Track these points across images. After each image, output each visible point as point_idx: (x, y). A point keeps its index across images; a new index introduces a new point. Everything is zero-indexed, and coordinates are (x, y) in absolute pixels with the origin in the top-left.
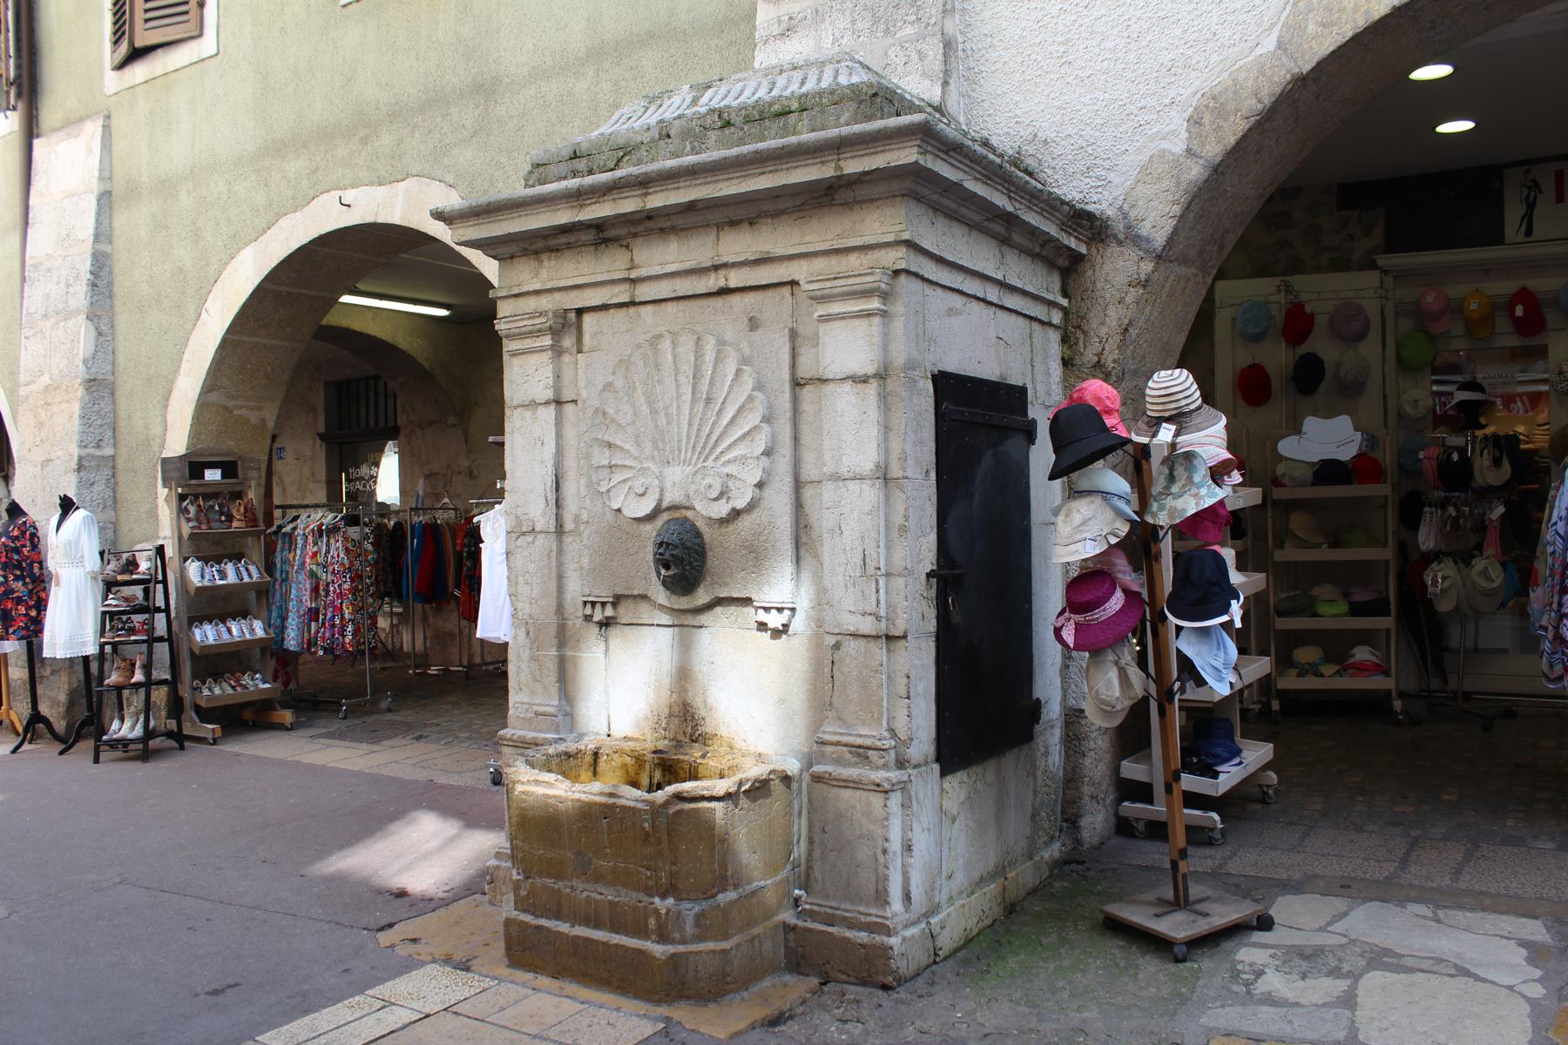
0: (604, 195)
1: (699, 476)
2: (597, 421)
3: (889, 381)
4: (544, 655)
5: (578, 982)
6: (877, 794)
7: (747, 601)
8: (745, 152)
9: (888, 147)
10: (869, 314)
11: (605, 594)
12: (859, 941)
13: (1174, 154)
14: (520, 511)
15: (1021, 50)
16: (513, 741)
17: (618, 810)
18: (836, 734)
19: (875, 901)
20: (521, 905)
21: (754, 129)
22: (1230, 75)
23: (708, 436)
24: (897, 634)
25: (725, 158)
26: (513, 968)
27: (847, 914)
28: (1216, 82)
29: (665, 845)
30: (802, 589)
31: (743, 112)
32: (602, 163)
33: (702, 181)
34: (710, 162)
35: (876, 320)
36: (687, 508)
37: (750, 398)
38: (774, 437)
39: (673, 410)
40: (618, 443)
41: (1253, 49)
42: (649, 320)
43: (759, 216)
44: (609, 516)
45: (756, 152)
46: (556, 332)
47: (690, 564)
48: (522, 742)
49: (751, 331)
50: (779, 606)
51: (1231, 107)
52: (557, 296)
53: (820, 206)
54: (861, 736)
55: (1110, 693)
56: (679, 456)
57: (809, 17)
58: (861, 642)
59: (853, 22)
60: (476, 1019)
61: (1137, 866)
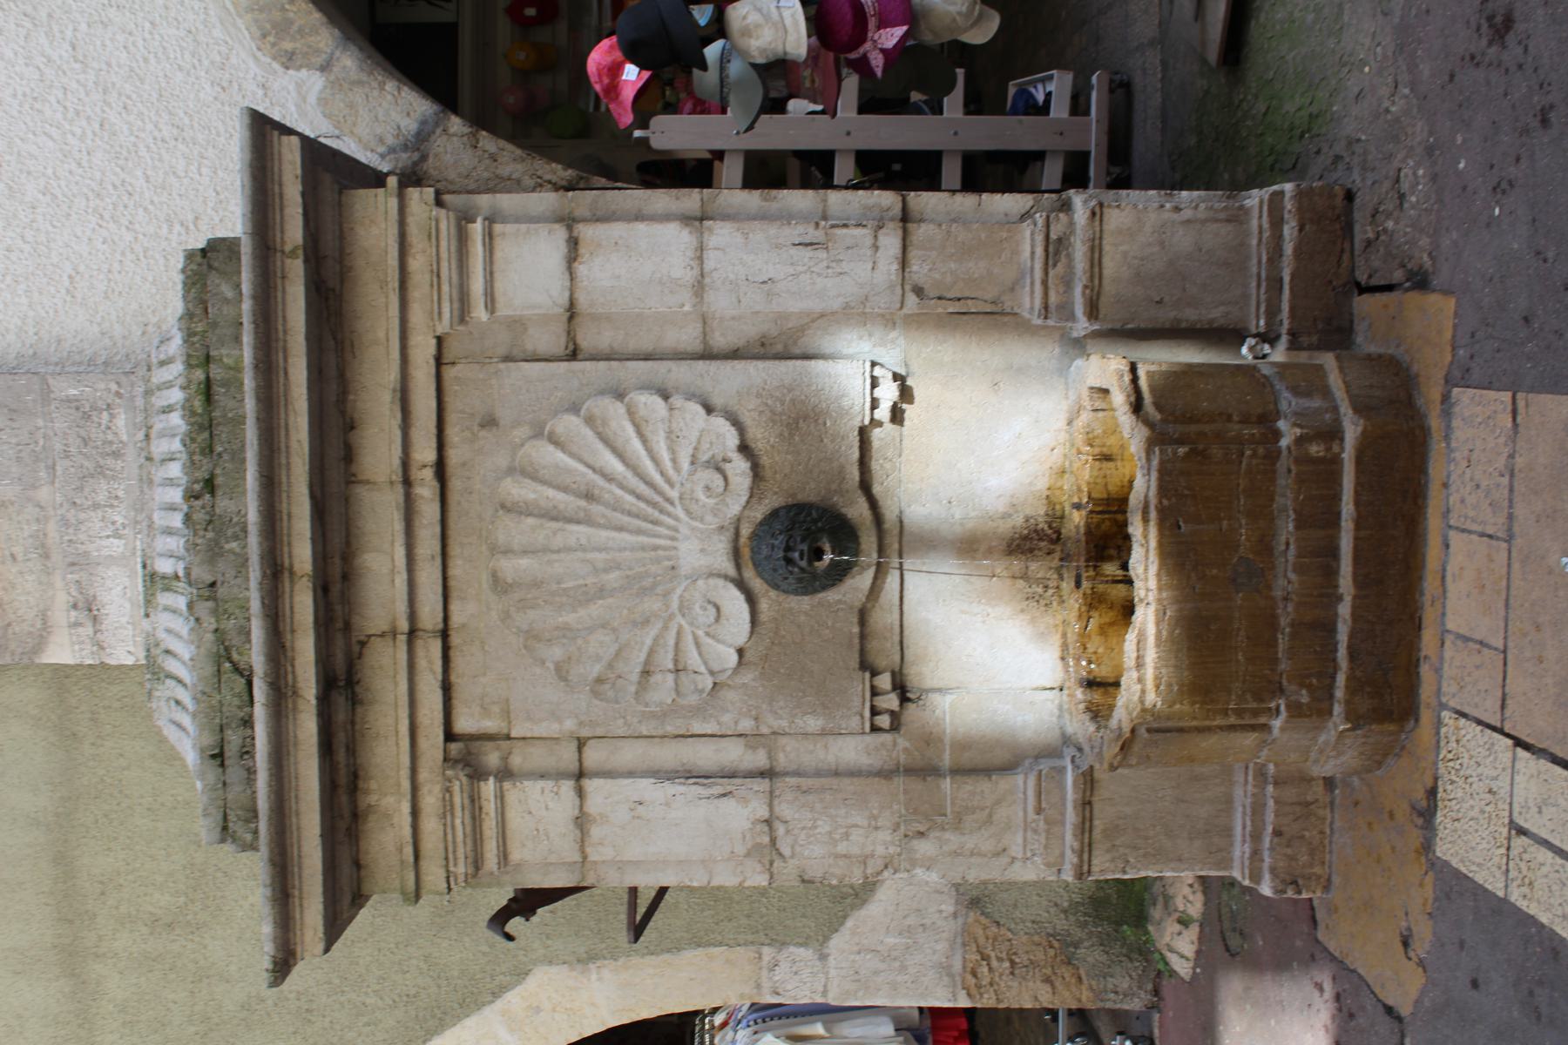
1: (694, 507)
2: (610, 694)
3: (577, 213)
4: (953, 804)
5: (1420, 578)
7: (863, 433)
9: (276, 178)
10: (489, 236)
11: (858, 686)
12: (1296, 233)
13: (325, 87)
14: (740, 849)
15: (170, 284)
17: (1165, 502)
18: (1032, 292)
20: (1320, 710)
21: (223, 432)
22: (240, 16)
25: (258, 419)
28: (246, 33)
29: (1207, 428)
30: (849, 17)
31: (197, 458)
32: (236, 702)
33: (284, 472)
34: (260, 444)
35: (498, 228)
36: (737, 534)
37: (590, 421)
38: (646, 387)
40: (643, 656)
43: (343, 413)
44: (747, 677)
45: (256, 367)
46: (477, 774)
47: (815, 521)
50: (868, 381)
51: (277, 15)
52: (424, 775)
54: (1033, 253)
56: (665, 548)
57: (76, 577)
58: (913, 253)
59: (96, 506)
60: (1505, 664)
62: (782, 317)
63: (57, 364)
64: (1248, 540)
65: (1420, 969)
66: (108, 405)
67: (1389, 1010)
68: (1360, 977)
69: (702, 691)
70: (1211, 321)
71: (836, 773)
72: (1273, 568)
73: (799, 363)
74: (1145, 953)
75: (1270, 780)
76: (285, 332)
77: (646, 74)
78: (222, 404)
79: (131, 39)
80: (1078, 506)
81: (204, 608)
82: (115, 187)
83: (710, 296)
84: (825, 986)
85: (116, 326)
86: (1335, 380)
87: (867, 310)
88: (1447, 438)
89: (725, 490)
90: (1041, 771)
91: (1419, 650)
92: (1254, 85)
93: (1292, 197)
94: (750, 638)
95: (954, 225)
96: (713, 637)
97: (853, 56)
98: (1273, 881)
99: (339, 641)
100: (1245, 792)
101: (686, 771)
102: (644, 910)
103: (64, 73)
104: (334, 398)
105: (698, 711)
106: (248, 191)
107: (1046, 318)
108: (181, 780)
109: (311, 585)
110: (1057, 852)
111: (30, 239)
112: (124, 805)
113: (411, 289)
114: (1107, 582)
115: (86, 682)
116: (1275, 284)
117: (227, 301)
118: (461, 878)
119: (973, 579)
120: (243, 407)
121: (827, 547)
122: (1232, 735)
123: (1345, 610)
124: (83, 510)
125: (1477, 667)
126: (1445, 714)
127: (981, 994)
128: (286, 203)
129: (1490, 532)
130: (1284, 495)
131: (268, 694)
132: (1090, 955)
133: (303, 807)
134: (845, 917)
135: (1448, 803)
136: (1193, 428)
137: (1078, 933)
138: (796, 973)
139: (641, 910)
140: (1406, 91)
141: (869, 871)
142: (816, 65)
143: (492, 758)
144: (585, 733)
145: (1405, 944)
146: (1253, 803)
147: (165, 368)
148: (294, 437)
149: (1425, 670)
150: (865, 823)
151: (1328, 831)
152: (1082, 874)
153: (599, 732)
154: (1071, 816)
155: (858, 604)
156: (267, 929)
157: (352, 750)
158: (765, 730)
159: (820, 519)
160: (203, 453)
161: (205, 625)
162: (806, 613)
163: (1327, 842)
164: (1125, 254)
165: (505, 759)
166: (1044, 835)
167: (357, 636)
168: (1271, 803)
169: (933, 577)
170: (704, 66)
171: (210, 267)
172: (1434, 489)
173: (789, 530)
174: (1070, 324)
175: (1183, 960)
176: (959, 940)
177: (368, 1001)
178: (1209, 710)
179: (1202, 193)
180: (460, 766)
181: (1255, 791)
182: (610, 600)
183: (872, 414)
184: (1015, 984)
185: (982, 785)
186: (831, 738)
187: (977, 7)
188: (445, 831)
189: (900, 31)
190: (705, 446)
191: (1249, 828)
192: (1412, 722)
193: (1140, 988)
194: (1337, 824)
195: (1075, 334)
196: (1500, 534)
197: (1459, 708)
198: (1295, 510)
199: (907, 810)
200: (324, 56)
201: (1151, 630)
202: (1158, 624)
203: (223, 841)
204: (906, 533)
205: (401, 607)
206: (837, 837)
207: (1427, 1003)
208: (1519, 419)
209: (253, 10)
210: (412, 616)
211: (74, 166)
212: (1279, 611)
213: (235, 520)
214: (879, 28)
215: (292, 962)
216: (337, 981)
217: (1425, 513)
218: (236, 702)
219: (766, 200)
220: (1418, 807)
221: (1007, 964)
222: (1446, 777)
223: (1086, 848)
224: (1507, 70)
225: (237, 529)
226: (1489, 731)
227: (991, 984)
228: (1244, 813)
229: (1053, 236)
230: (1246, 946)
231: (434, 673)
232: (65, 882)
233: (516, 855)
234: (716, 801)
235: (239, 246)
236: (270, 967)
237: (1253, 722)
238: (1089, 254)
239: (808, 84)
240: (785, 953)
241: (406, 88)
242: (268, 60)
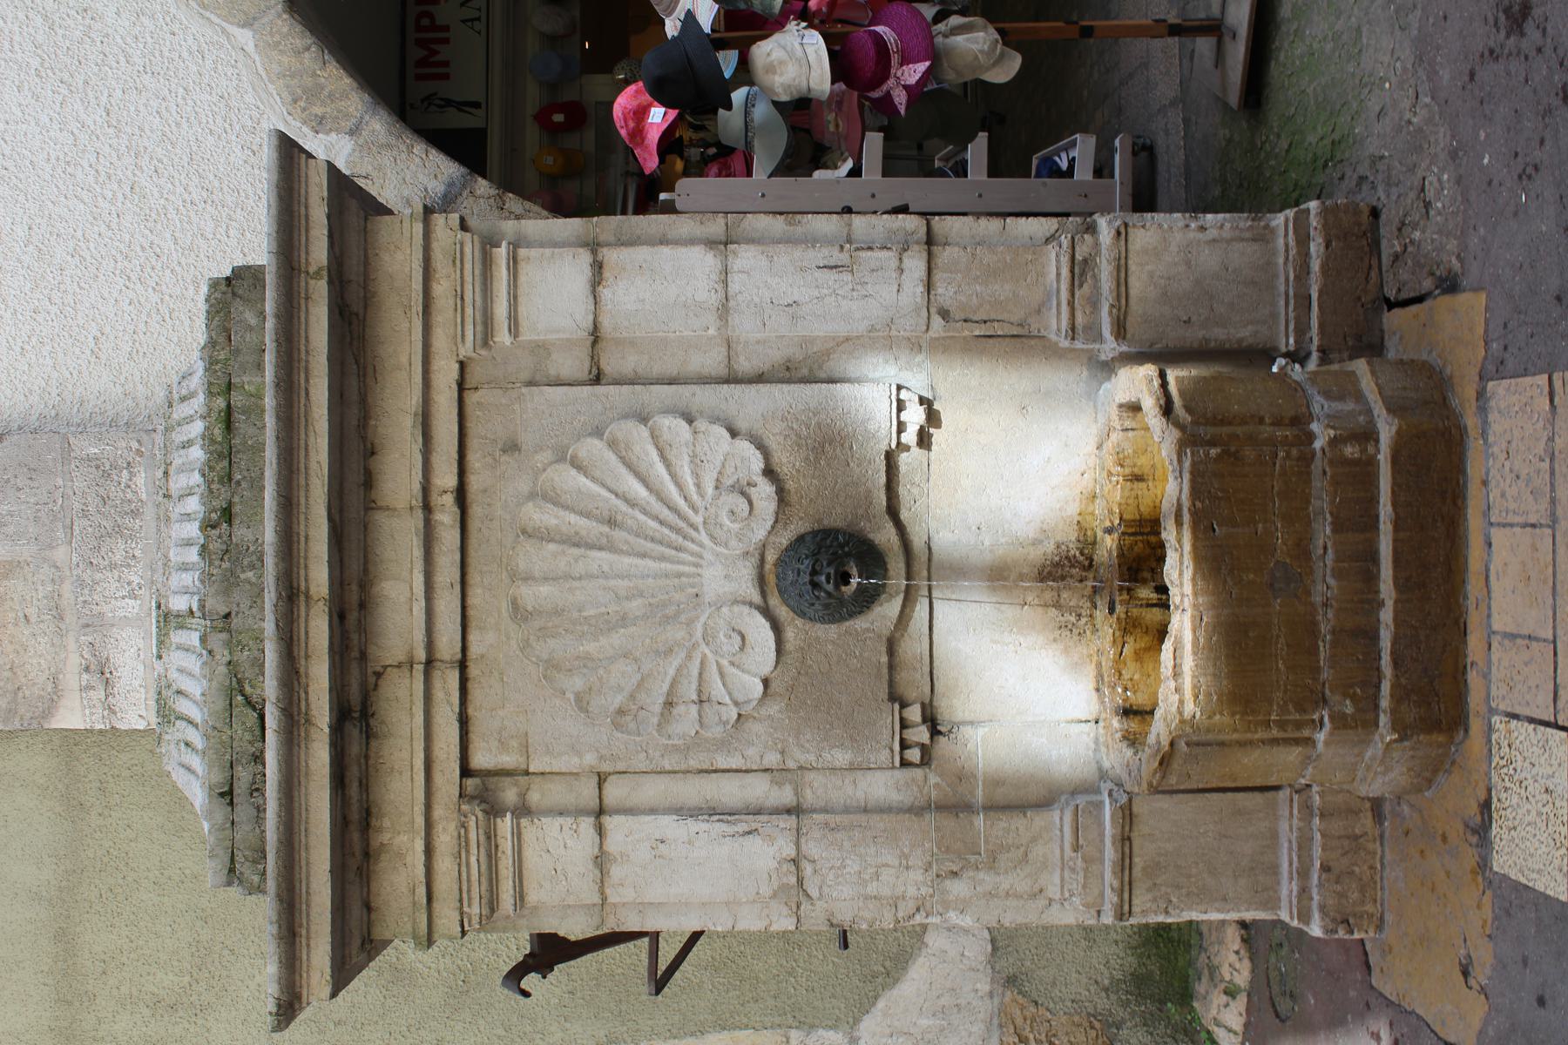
1: (718, 532)
2: (632, 726)
3: (602, 238)
4: (986, 842)
6: (1130, 239)
7: (890, 458)
8: (274, 403)
9: (303, 200)
10: (514, 261)
11: (887, 718)
12: (1322, 249)
13: (354, 150)
14: (766, 891)
17: (1199, 504)
18: (1059, 313)
19: (1268, 242)
20: (1365, 721)
21: (242, 460)
22: (272, 82)
23: (661, 523)
24: (925, 228)
25: (278, 438)
26: (1467, 717)
28: (278, 98)
29: (1239, 430)
30: (872, 53)
32: (248, 736)
33: (302, 493)
35: (522, 252)
36: (762, 560)
37: (613, 444)
39: (622, 584)
40: (666, 687)
42: (490, 637)
43: (364, 439)
44: (773, 708)
45: (277, 385)
46: (494, 811)
47: (842, 546)
48: (1122, 870)
51: (308, 81)
52: (438, 812)
53: (363, 339)
54: (1058, 275)
55: (981, 41)
56: (688, 575)
57: (90, 639)
58: (938, 276)
59: (113, 566)
60: (1555, 654)
61: (1186, 193)
62: (806, 341)
65: (1483, 997)
66: (129, 463)
68: (1419, 1017)
69: (725, 723)
70: (1240, 341)
71: (865, 810)
72: (1312, 572)
77: (673, 114)
78: (242, 431)
79: (164, 105)
80: (1109, 531)
81: (217, 640)
82: (143, 249)
83: (735, 319)
85: (140, 387)
86: (1367, 384)
87: (894, 333)
88: (1484, 435)
91: (1466, 656)
92: (1275, 124)
94: (775, 667)
96: (738, 667)
97: (876, 94)
101: (709, 808)
104: (355, 423)
105: (722, 745)
106: (274, 211)
107: (1073, 339)
109: (327, 609)
110: (1096, 892)
115: (96, 749)
116: (1304, 301)
117: (251, 329)
118: (476, 920)
119: (1004, 607)
120: (264, 434)
121: (854, 571)
123: (1386, 615)
124: (99, 570)
126: (1496, 719)
128: (311, 224)
129: (1532, 520)
130: (1320, 498)
131: (279, 721)
133: (313, 841)
136: (1225, 430)
137: (1121, 1013)
139: (663, 966)
140: (1427, 100)
141: (900, 915)
142: (840, 109)
143: (510, 795)
144: (606, 767)
145: (1465, 973)
146: (1299, 838)
147: (186, 403)
149: (1473, 677)
152: (1122, 914)
153: (621, 766)
154: (1110, 853)
155: (886, 633)
156: (272, 969)
157: (365, 786)
158: (791, 764)
159: (847, 543)
160: (221, 482)
161: (218, 657)
165: (522, 796)
166: (1082, 874)
167: (374, 666)
168: (1318, 836)
169: (963, 606)
170: (729, 106)
171: (234, 294)
172: (1473, 489)
173: (815, 555)
174: (1097, 346)
175: (1231, 1035)
176: (996, 1021)
179: (1228, 215)
180: (477, 802)
182: (632, 629)
185: (1018, 822)
186: (859, 773)
187: (999, 46)
189: (922, 67)
190: (729, 470)
194: (1388, 857)
195: (1103, 357)
196: (1543, 522)
197: (1509, 710)
198: (1331, 514)
199: (939, 849)
201: (1188, 637)
202: (1194, 631)
203: (229, 884)
205: (419, 636)
206: (867, 877)
208: (1556, 400)
210: (430, 645)
211: (103, 228)
212: (1320, 618)
213: (252, 549)
214: (902, 65)
217: (1465, 515)
218: (248, 736)
220: (1471, 824)
222: (1500, 785)
223: (1126, 887)
224: (1526, 58)
225: (254, 558)
226: (1542, 728)
228: (1290, 849)
229: (1079, 257)
230: (1296, 1009)
233: (532, 897)
234: (741, 839)
235: (264, 274)
236: (274, 1010)
237: (1297, 735)
238: (1115, 273)
239: (832, 128)
242: (299, 125)
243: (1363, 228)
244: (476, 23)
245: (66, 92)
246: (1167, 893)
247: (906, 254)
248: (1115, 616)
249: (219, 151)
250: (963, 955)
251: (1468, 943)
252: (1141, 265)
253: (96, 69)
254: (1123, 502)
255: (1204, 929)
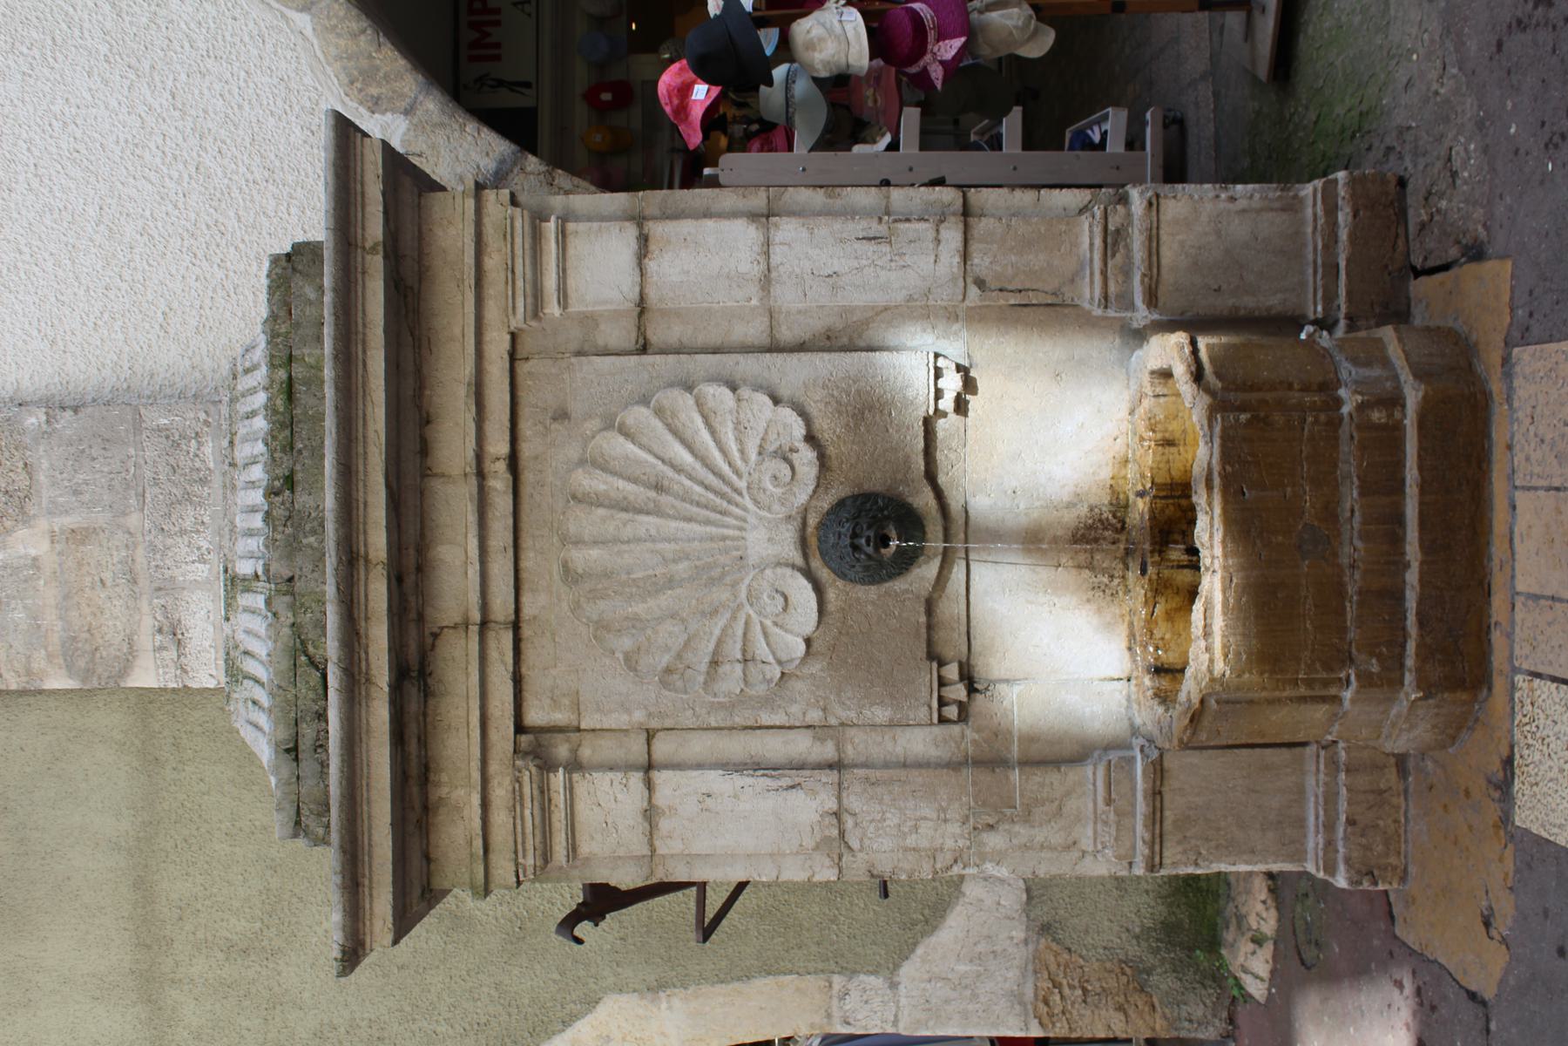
0: (358, 634)
1: (761, 497)
2: (679, 684)
3: (647, 212)
4: (1022, 795)
7: (928, 423)
9: (359, 178)
10: (563, 235)
11: (926, 677)
12: (1350, 218)
13: (409, 130)
14: (809, 843)
16: (1153, 843)
17: (1229, 468)
18: (1092, 282)
19: (1296, 212)
20: (1390, 680)
21: (303, 430)
25: (337, 408)
26: (1491, 676)
27: (1320, 246)
29: (1269, 396)
30: (909, 29)
32: (311, 695)
33: (361, 462)
34: (338, 433)
35: (571, 226)
37: (659, 412)
40: (711, 646)
41: (305, 38)
42: (542, 599)
43: (419, 408)
44: (815, 667)
45: (336, 357)
46: (546, 765)
47: (881, 510)
48: (1154, 824)
49: (569, 419)
51: (364, 63)
52: (494, 767)
54: (1092, 245)
56: (733, 539)
57: (162, 602)
58: (974, 247)
59: (183, 532)
62: (846, 311)
63: (149, 397)
64: (1313, 506)
65: (1504, 947)
66: (197, 434)
67: (1472, 996)
68: (1441, 966)
69: (769, 681)
70: (1269, 309)
71: (905, 765)
73: (864, 354)
74: (1220, 980)
75: (1342, 767)
76: (364, 325)
77: (716, 91)
79: (227, 87)
80: (1141, 494)
81: (281, 603)
82: (208, 226)
83: (776, 290)
84: (896, 1016)
85: (206, 360)
86: (1394, 351)
87: (931, 302)
88: (1509, 400)
89: (792, 479)
90: (1110, 761)
91: (1490, 616)
93: (1345, 184)
94: (818, 627)
95: (1014, 219)
97: (913, 70)
98: (1348, 871)
99: (413, 632)
100: (1317, 781)
102: (711, 916)
103: (164, 120)
104: (410, 393)
105: (767, 702)
106: (331, 189)
107: (1106, 307)
108: (259, 804)
110: (1128, 844)
111: (128, 278)
112: (203, 830)
113: (486, 286)
114: (1172, 567)
115: (169, 707)
116: (1332, 269)
117: (310, 303)
118: (530, 871)
119: (1039, 569)
122: (1303, 707)
123: (1412, 577)
124: (170, 536)
125: (1549, 624)
126: (1519, 678)
127: (1053, 1024)
129: (1556, 484)
130: (1347, 462)
131: (341, 680)
132: (1163, 981)
133: (374, 795)
134: (915, 944)
135: (1526, 769)
137: (1151, 960)
138: (866, 1002)
139: (710, 914)
140: (1455, 71)
141: (938, 866)
143: (562, 751)
144: (654, 724)
147: (249, 375)
148: (371, 427)
149: (1497, 637)
150: (935, 816)
151: (1403, 820)
153: (668, 723)
154: (1141, 807)
155: (925, 594)
157: (423, 741)
158: (833, 721)
160: (284, 450)
161: (282, 619)
162: (873, 603)
163: (1402, 831)
164: (1182, 244)
165: (574, 751)
167: (431, 627)
168: (1344, 791)
169: (999, 567)
170: (770, 83)
171: (294, 269)
173: (855, 518)
176: (1030, 967)
177: (439, 1029)
178: (1278, 680)
181: (1327, 779)
182: (679, 591)
183: (936, 404)
184: (1088, 1013)
185: (1053, 777)
186: (899, 730)
187: (1033, 22)
188: (514, 824)
189: (958, 43)
190: (772, 436)
191: (1321, 819)
192: (1485, 691)
193: (1215, 1016)
194: (1412, 812)
195: (1135, 325)
197: (1532, 669)
198: (1359, 477)
199: (976, 803)
200: (408, 100)
201: (1218, 597)
202: (1224, 592)
203: (295, 835)
204: (971, 523)
205: (474, 598)
206: (906, 830)
207: (1512, 982)
209: (341, 58)
210: (484, 606)
213: (313, 515)
214: (938, 41)
215: (361, 953)
216: (408, 1009)
217: (1490, 479)
219: (830, 197)
220: (1494, 780)
221: (1079, 992)
222: (1523, 742)
223: (1157, 840)
224: (1554, 27)
225: (315, 523)
227: (1063, 1013)
228: (1317, 803)
229: (1111, 227)
231: (505, 665)
232: (144, 907)
233: (585, 849)
236: (339, 956)
237: (1324, 693)
239: (870, 103)
240: (855, 982)
241: (485, 130)
242: (356, 105)
243: (1390, 198)
244: (526, 6)
245: (134, 77)
246: (1197, 846)
247: (943, 225)
248: (1147, 577)
249: (280, 132)
250: (999, 904)
251: (1490, 894)
252: (1172, 235)
253: (161, 54)
254: (1155, 466)
255: (1232, 879)
